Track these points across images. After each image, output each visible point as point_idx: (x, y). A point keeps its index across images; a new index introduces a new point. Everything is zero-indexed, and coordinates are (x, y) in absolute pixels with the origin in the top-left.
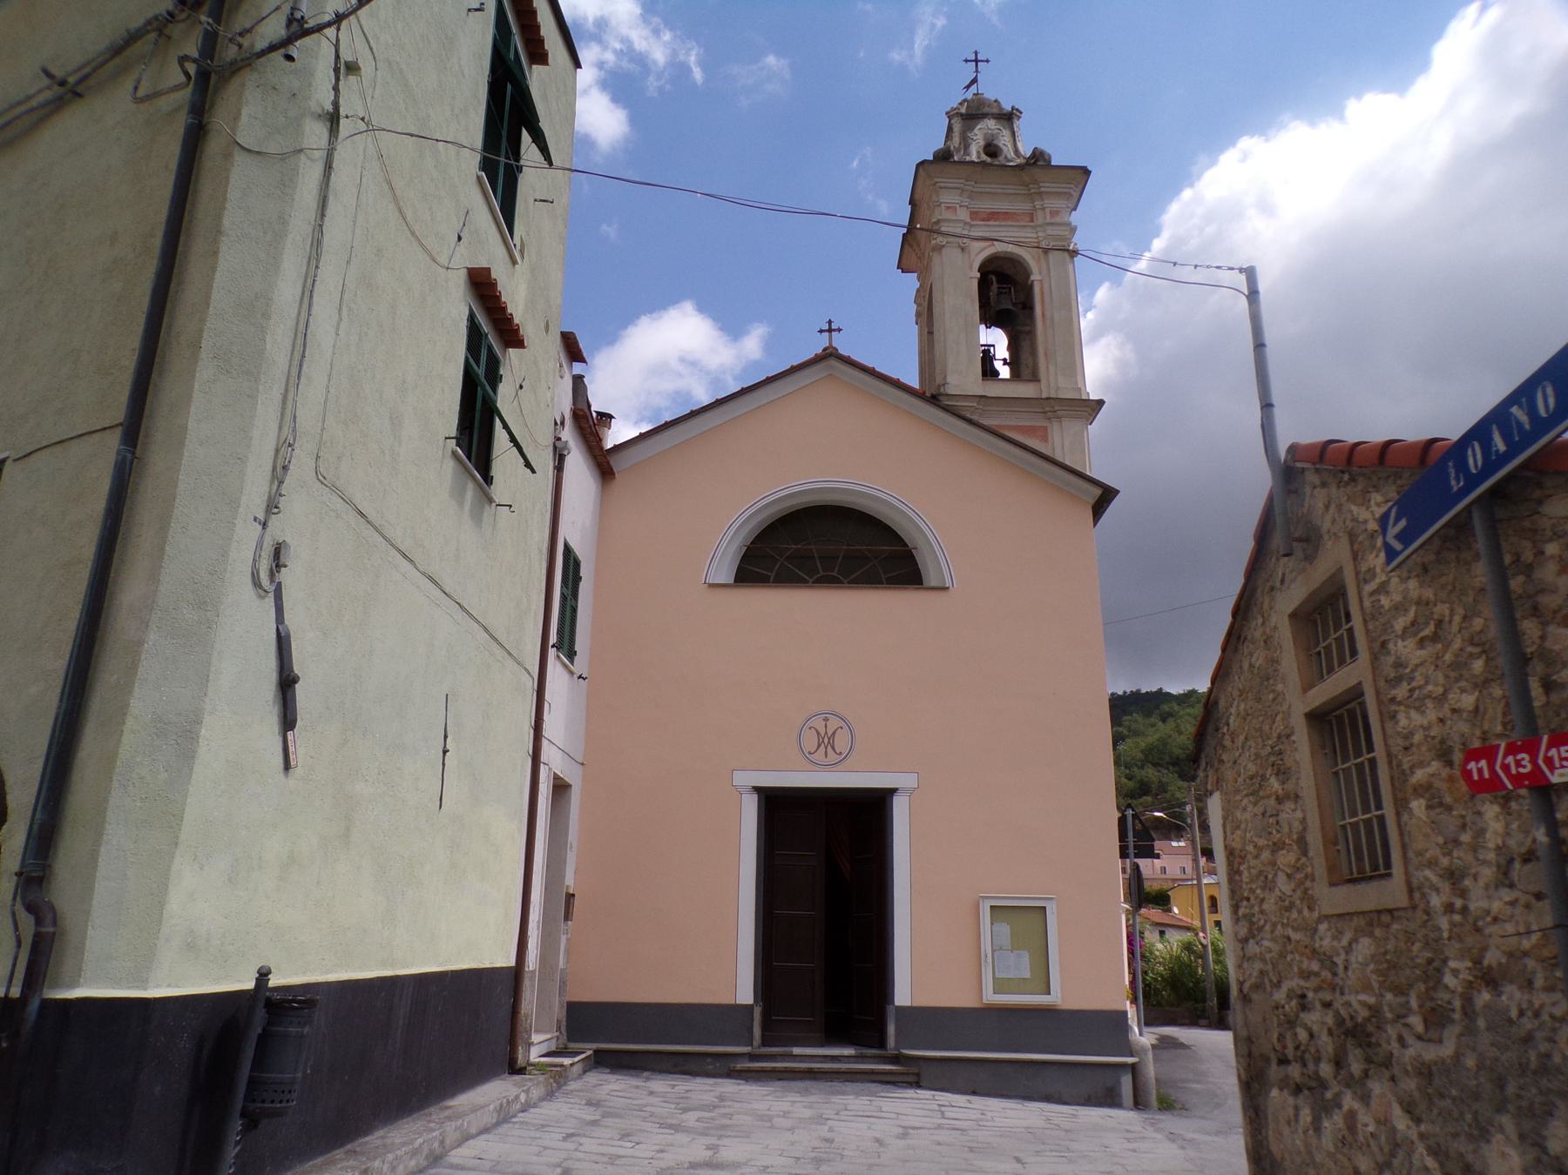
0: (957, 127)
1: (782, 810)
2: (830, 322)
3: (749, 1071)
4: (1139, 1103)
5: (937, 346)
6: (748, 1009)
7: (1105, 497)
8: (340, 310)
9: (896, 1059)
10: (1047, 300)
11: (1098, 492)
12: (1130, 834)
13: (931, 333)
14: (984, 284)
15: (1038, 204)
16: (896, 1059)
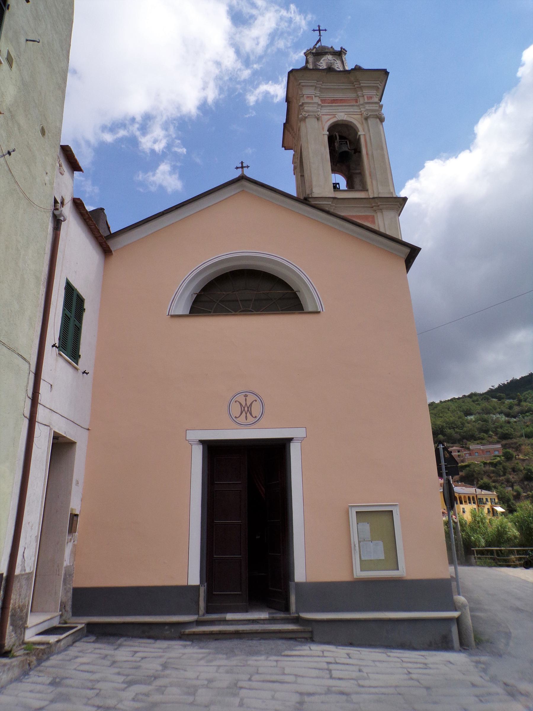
0: (311, 60)
1: (219, 455)
2: (242, 163)
3: (194, 634)
4: (464, 646)
5: (307, 184)
6: (196, 588)
7: (413, 252)
9: (297, 620)
10: (369, 144)
11: (407, 251)
12: (443, 460)
13: (302, 176)
14: (331, 139)
15: (360, 93)
16: (297, 620)
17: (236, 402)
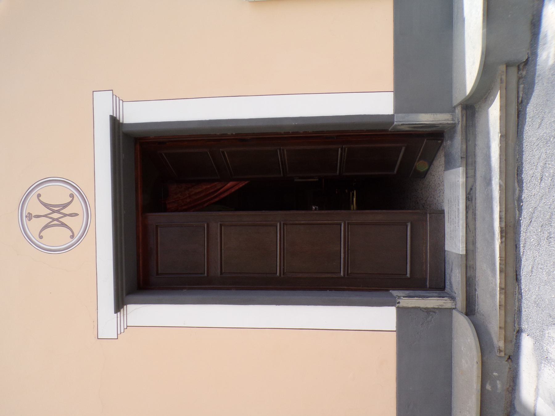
1: (143, 274)
6: (402, 313)
8: (296, 224)
16: (472, 108)
17: (41, 237)
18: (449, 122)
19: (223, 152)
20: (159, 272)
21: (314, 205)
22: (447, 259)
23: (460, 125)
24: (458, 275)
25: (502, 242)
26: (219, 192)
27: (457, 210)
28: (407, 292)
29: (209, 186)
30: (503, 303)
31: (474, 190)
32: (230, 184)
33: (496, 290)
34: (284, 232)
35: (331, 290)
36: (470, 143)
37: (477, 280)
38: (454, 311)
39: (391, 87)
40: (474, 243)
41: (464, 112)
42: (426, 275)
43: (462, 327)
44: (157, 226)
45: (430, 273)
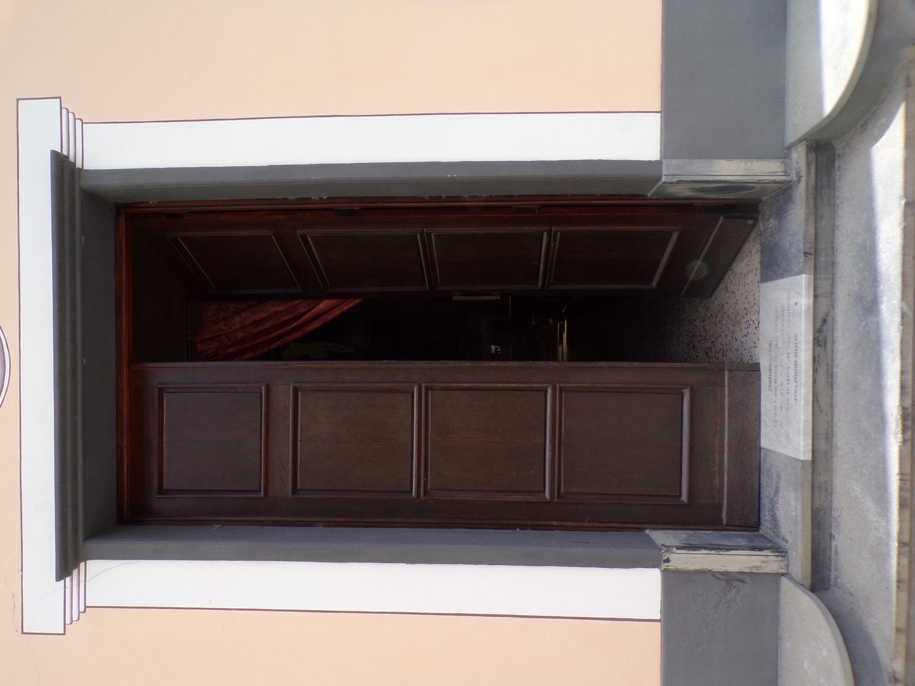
1: (121, 496)
6: (676, 586)
8: (454, 389)
18: (778, 178)
19: (304, 237)
20: (165, 487)
21: (494, 344)
22: (765, 466)
23: (802, 185)
24: (793, 503)
25: (904, 441)
26: (303, 319)
27: (792, 366)
28: (683, 535)
29: (281, 308)
30: (905, 576)
31: (829, 322)
32: (323, 305)
33: (887, 545)
34: (427, 405)
35: (523, 527)
36: (824, 222)
37: (835, 514)
38: (784, 581)
39: (655, 100)
40: (829, 436)
41: (813, 156)
42: (721, 499)
43: (803, 614)
44: (161, 391)
45: (729, 494)
